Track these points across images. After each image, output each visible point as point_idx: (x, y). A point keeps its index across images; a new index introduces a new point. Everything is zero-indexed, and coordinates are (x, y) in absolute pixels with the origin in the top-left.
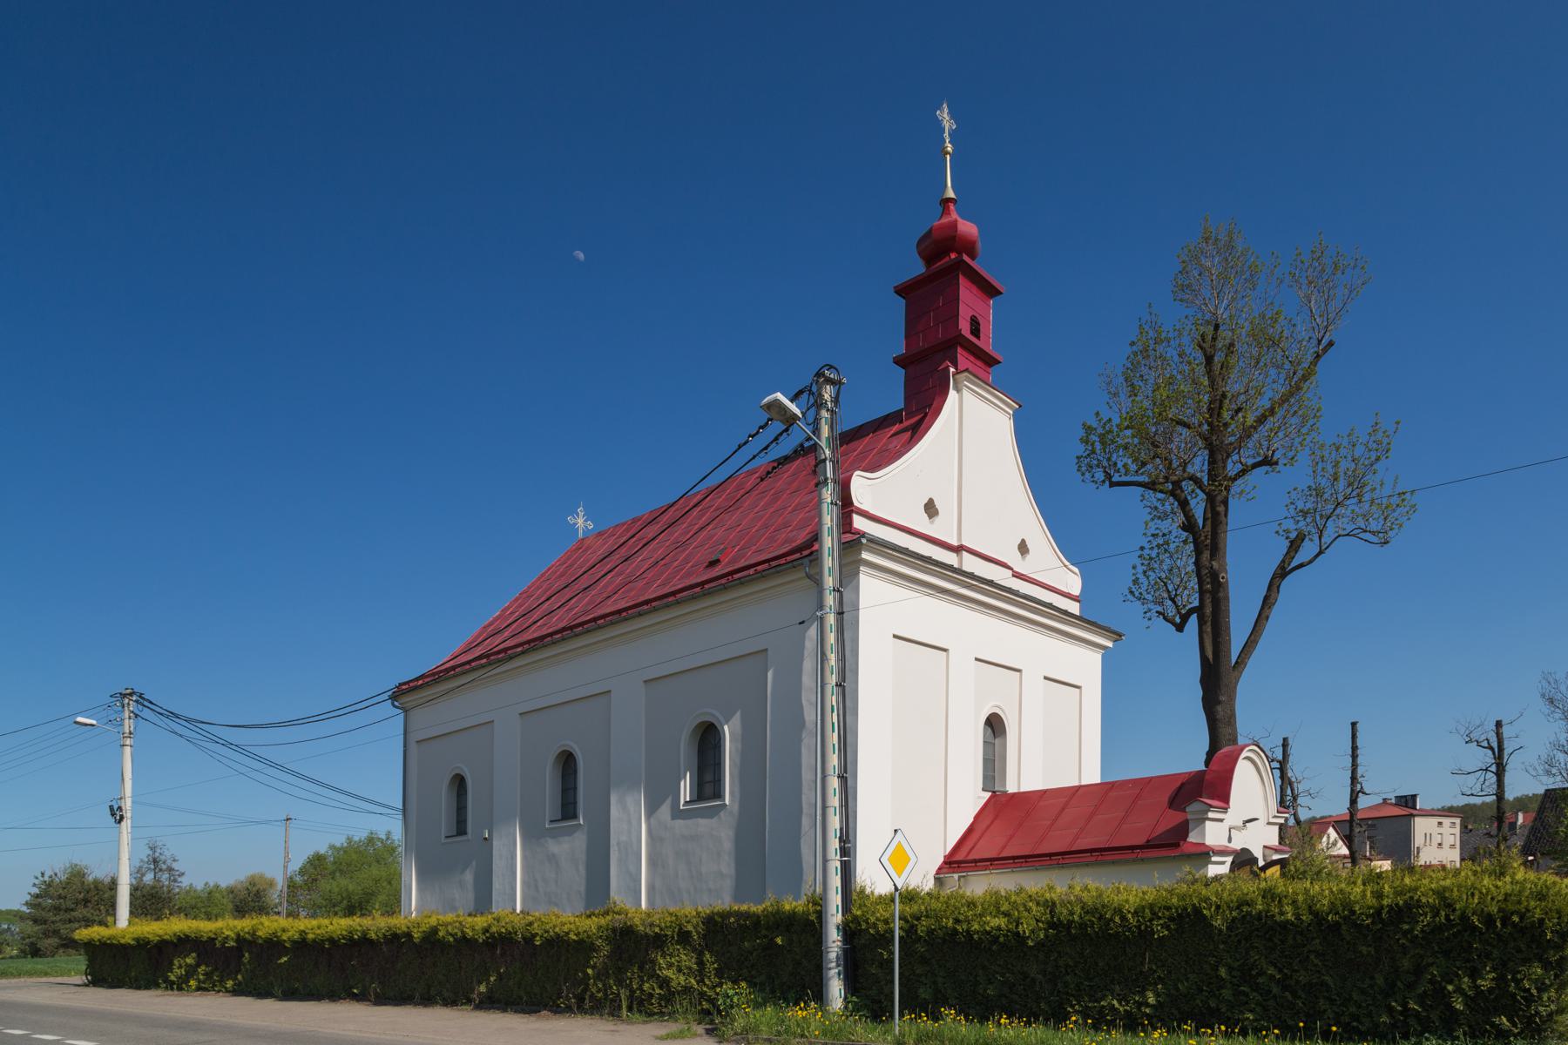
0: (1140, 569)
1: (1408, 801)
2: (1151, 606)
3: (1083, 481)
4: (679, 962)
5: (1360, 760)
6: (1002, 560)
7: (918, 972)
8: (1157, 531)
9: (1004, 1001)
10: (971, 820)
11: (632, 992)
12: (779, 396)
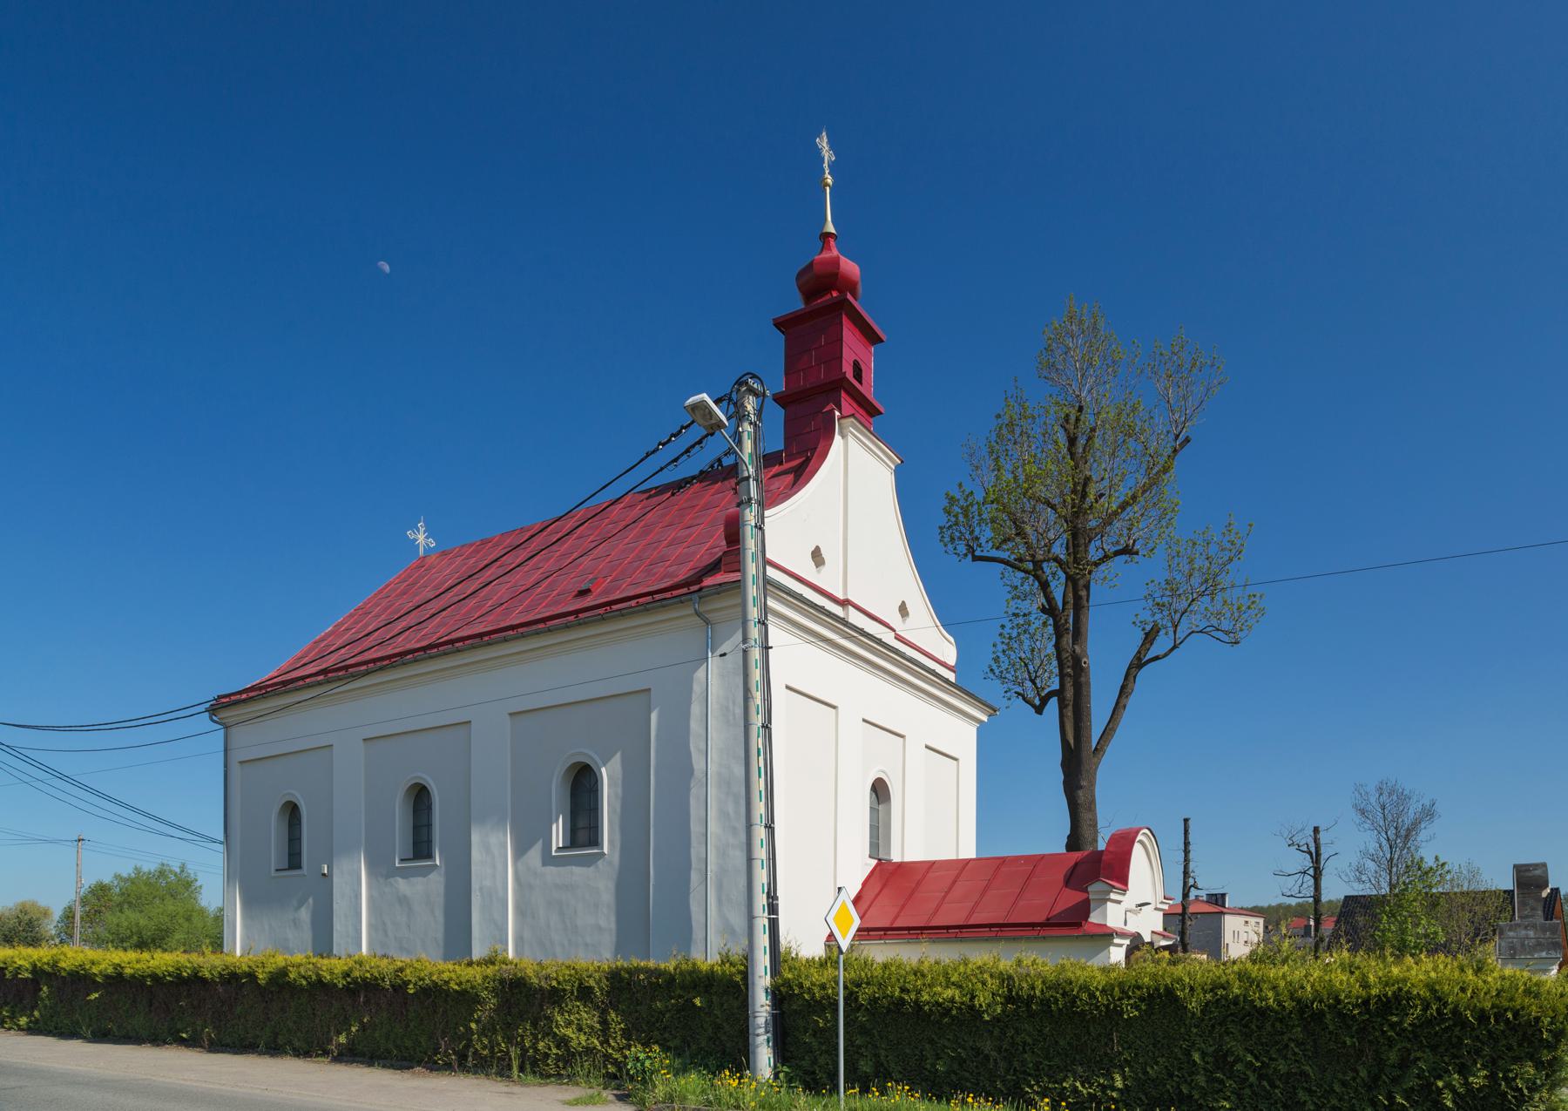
1: (1218, 899)
3: (946, 552)
4: (578, 1020)
5: (1191, 856)
8: (1017, 611)
9: (954, 1077)
11: (524, 1050)
12: (705, 396)
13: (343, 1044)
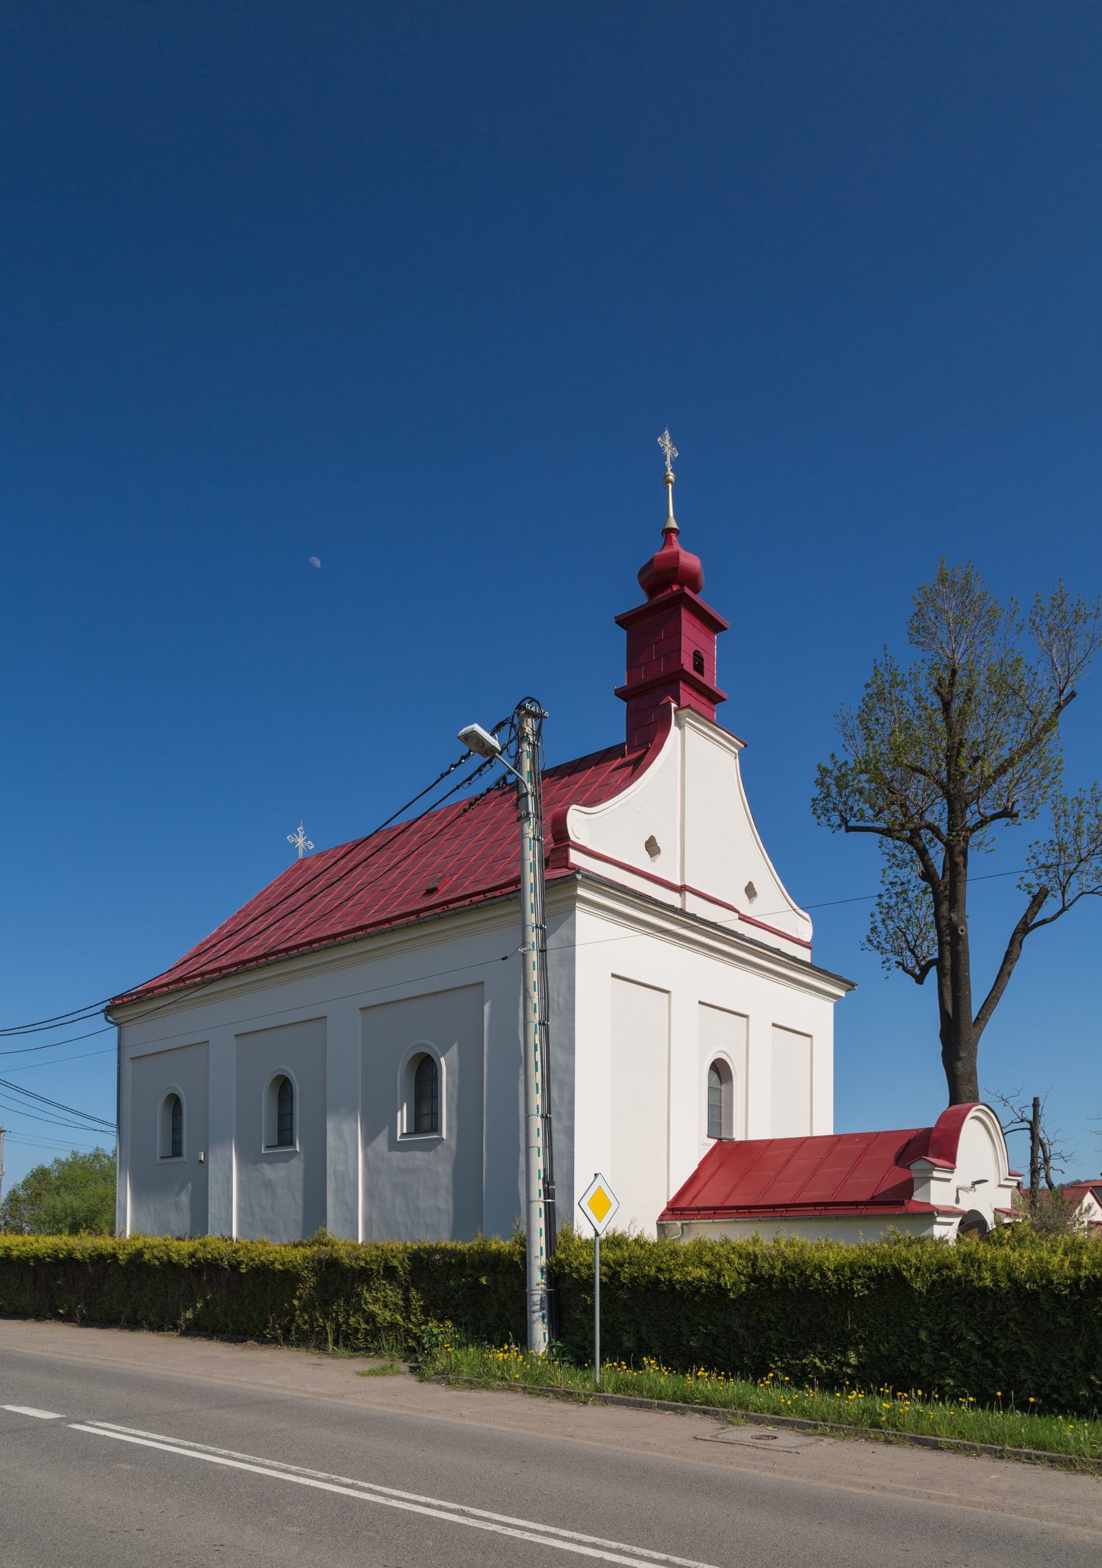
0: (879, 918)
2: (890, 956)
3: (818, 824)
4: (384, 1297)
6: (722, 900)
7: (622, 1319)
10: (696, 1167)
11: (338, 1325)
12: (477, 727)
13: (190, 1319)
